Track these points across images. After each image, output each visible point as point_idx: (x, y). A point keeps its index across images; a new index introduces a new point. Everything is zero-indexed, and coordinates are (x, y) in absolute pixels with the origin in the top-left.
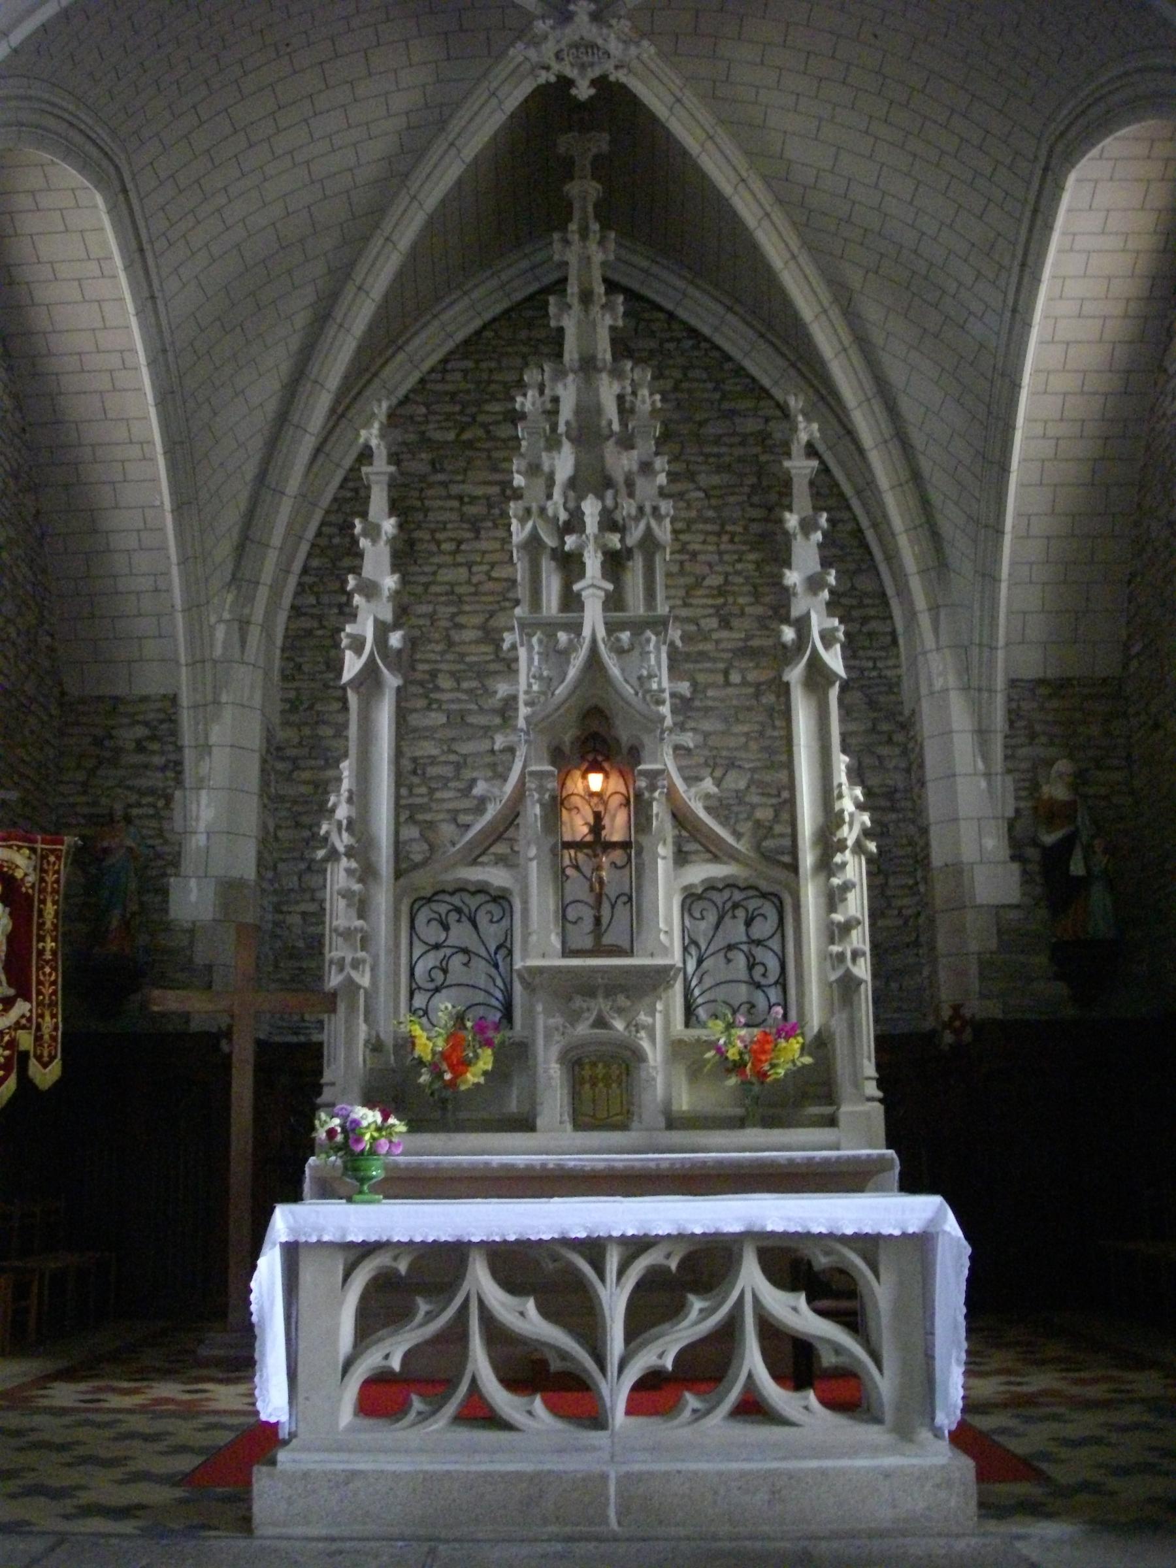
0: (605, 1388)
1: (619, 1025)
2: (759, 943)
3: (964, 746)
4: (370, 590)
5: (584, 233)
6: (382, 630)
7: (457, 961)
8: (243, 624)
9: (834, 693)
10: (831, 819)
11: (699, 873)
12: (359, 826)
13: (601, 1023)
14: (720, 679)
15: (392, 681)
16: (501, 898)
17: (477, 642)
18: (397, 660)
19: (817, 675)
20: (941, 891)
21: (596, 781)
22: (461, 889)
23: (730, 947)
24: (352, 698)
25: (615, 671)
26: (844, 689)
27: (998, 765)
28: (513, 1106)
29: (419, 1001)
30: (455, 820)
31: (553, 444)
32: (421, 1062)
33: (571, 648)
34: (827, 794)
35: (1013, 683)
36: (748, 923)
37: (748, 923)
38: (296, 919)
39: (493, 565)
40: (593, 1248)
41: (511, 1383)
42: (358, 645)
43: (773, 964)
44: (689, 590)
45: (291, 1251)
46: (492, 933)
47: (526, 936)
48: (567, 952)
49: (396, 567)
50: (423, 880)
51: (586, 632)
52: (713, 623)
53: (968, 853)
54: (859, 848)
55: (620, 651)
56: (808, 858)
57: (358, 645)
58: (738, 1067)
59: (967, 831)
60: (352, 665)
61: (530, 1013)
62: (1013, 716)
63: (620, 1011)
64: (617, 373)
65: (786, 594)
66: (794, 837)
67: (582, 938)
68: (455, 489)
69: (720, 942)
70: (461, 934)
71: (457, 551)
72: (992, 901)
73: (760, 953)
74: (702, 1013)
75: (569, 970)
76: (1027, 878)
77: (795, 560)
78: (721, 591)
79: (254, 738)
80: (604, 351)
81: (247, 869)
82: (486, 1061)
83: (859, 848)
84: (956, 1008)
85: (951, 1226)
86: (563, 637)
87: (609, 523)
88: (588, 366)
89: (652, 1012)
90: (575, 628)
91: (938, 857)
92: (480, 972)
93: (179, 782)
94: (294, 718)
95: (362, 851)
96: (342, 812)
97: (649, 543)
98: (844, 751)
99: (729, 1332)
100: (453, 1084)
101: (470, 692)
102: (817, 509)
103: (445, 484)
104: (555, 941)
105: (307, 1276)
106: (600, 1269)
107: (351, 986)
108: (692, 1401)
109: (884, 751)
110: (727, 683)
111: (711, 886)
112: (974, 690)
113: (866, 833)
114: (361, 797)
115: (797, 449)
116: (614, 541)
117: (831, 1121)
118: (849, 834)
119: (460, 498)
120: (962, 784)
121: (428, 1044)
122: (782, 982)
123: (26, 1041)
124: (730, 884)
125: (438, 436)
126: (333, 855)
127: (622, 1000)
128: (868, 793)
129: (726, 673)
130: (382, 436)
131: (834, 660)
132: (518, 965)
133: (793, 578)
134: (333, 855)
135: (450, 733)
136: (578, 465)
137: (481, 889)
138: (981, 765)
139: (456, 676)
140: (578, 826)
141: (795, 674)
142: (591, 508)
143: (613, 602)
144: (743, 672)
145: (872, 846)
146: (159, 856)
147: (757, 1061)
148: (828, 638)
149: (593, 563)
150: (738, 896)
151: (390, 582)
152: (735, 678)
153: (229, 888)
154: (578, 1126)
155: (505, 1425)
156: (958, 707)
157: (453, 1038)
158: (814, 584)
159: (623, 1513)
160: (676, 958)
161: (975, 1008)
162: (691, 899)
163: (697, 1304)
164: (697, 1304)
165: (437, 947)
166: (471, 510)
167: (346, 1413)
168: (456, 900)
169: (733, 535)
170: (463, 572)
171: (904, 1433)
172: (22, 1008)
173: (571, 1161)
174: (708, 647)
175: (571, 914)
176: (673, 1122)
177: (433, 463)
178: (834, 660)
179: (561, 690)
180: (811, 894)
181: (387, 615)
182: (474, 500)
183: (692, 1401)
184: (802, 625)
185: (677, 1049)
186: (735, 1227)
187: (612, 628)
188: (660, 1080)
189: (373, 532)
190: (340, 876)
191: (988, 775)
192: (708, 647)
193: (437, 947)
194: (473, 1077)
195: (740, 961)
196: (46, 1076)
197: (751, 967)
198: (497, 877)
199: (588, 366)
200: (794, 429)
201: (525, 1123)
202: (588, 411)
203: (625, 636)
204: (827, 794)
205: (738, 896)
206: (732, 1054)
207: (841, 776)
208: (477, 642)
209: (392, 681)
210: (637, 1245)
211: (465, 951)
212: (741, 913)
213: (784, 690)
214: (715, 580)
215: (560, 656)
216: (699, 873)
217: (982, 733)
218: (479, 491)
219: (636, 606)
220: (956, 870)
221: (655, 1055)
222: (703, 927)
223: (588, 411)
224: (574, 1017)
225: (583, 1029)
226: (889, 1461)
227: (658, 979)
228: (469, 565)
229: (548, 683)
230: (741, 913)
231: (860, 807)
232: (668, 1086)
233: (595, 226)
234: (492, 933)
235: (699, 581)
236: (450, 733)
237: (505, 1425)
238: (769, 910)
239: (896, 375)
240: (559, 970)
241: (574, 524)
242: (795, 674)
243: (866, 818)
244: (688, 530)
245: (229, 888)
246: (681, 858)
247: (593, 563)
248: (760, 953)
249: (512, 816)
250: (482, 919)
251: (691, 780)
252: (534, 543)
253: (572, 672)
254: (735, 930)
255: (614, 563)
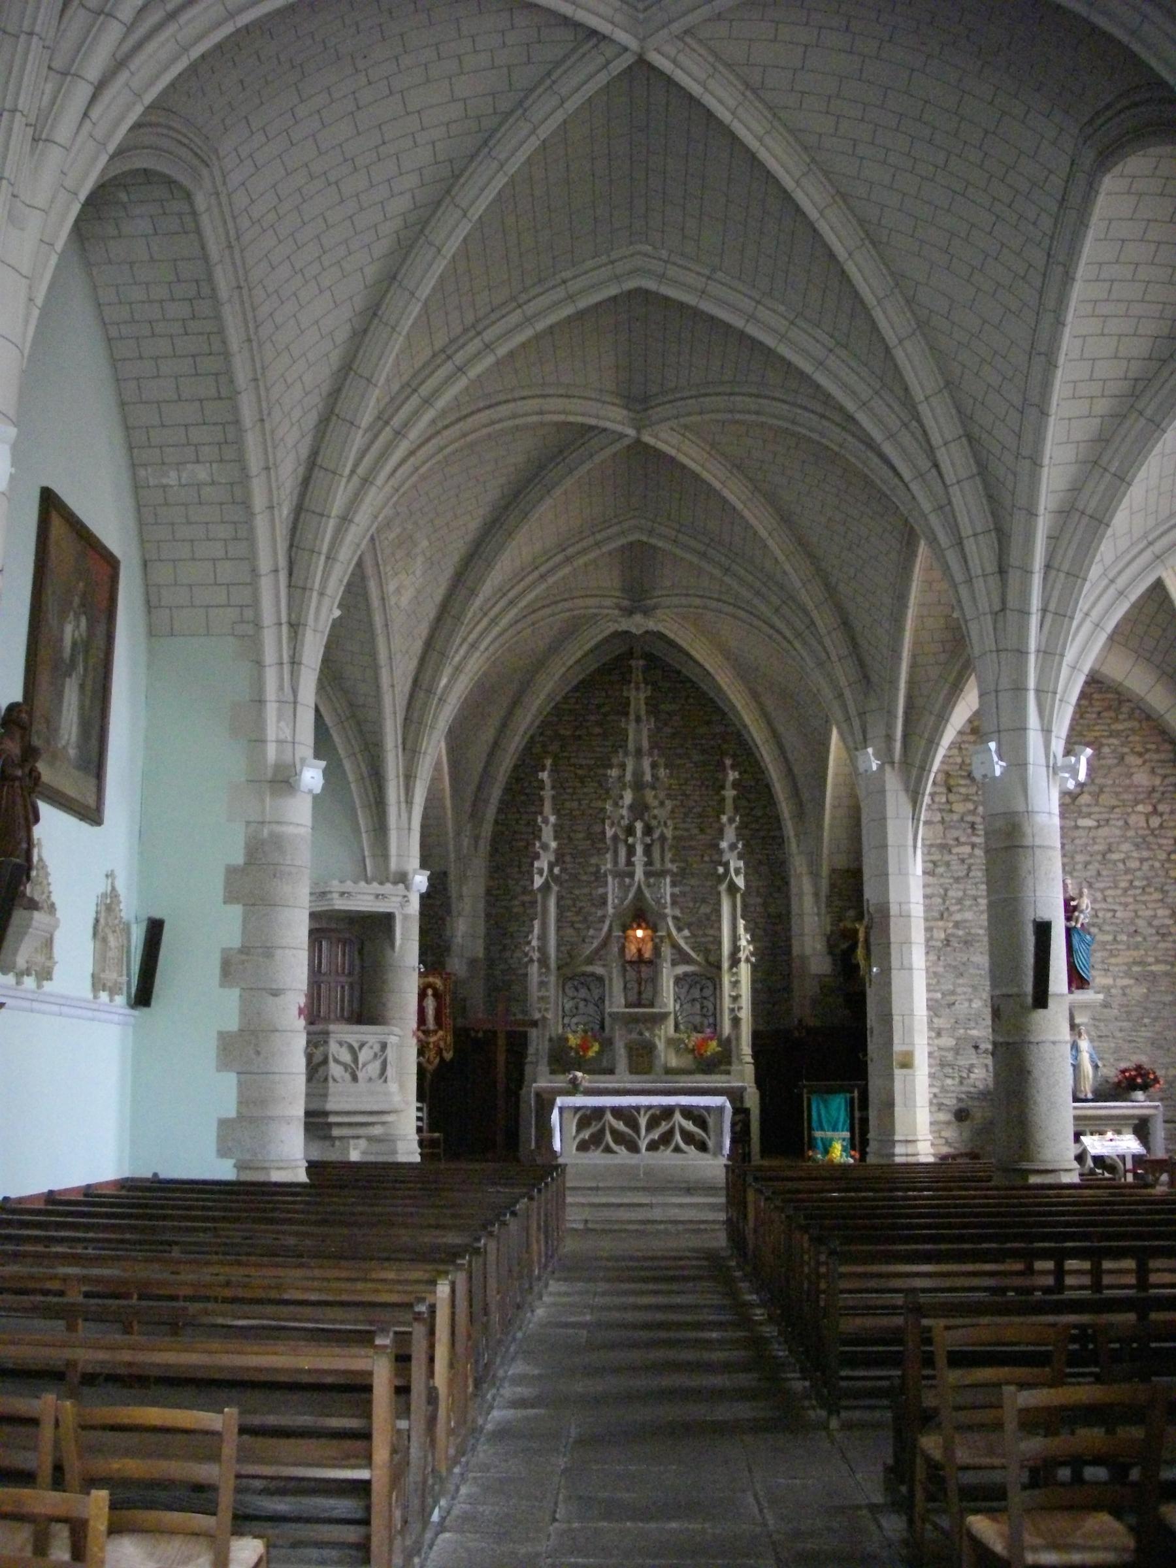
0: (640, 1143)
1: (647, 1034)
2: (705, 998)
3: (808, 903)
4: (545, 847)
5: (638, 689)
6: (551, 866)
7: (582, 1004)
8: (477, 838)
9: (739, 896)
10: (736, 949)
11: (681, 969)
12: (542, 949)
13: (641, 1034)
14: (698, 858)
15: (555, 888)
16: (600, 979)
17: (584, 839)
18: (556, 879)
19: (733, 889)
20: (796, 964)
21: (640, 933)
22: (584, 974)
23: (694, 1000)
24: (539, 897)
25: (648, 895)
26: (743, 896)
27: (823, 911)
28: (605, 1064)
29: (566, 1021)
30: (572, 926)
31: (623, 788)
32: (571, 1048)
33: (630, 886)
34: (735, 938)
35: (833, 871)
36: (701, 990)
37: (701, 990)
38: (498, 972)
39: (591, 801)
40: (637, 1109)
41: (616, 1142)
42: (541, 872)
43: (711, 1007)
44: (686, 815)
45: (561, 1109)
46: (596, 993)
47: (611, 996)
48: (626, 1006)
49: (556, 838)
50: (567, 971)
51: (636, 879)
52: (696, 831)
53: (808, 951)
54: (747, 960)
55: (649, 886)
56: (726, 965)
57: (541, 872)
58: (693, 1051)
59: (808, 941)
60: (538, 881)
61: (612, 1029)
62: (833, 886)
63: (648, 1029)
64: (651, 754)
65: (720, 852)
66: (720, 955)
67: (633, 997)
68: (572, 761)
69: (690, 997)
70: (583, 993)
71: (574, 793)
72: (819, 972)
73: (706, 1003)
74: (682, 1027)
75: (630, 1014)
76: (834, 963)
77: (725, 836)
78: (700, 816)
79: (481, 890)
80: (645, 745)
81: (481, 954)
82: (596, 1047)
83: (747, 960)
84: (800, 1021)
85: (728, 1104)
86: (627, 880)
87: (648, 831)
88: (639, 753)
89: (660, 1029)
90: (631, 875)
91: (796, 950)
92: (591, 1009)
93: (449, 912)
94: (496, 875)
95: (544, 962)
96: (535, 943)
97: (663, 838)
98: (743, 917)
99: (671, 1132)
100: (584, 1056)
101: (579, 863)
102: (735, 814)
103: (569, 758)
104: (623, 1001)
105: (565, 1115)
106: (639, 1113)
107: (544, 1018)
108: (662, 1148)
109: (776, 895)
110: (703, 862)
111: (686, 975)
112: (815, 875)
113: (752, 954)
114: (543, 937)
115: (728, 784)
116: (648, 840)
117: (728, 1073)
118: (742, 955)
119: (574, 765)
120: (807, 919)
121: (573, 1040)
122: (714, 1015)
123: (442, 1044)
124: (694, 974)
125: (562, 732)
126: (532, 960)
127: (649, 1025)
128: (752, 936)
129: (702, 856)
130: (549, 776)
131: (740, 882)
132: (608, 1010)
133: (724, 845)
134: (532, 960)
135: (571, 884)
136: (634, 799)
137: (593, 974)
138: (815, 910)
139: (574, 857)
140: (632, 949)
141: (723, 887)
142: (639, 826)
143: (649, 863)
144: (711, 856)
145: (753, 959)
146: (439, 946)
147: (699, 1049)
148: (737, 872)
149: (639, 849)
150: (697, 979)
151: (553, 845)
152: (706, 858)
153: (473, 962)
154: (631, 1072)
155: (615, 1152)
156: (807, 886)
157: (584, 1039)
158: (733, 847)
159: (645, 1174)
160: (671, 1009)
161: (812, 1022)
162: (678, 980)
163: (664, 1123)
164: (664, 1123)
165: (573, 998)
166: (580, 772)
167: (574, 1151)
168: (582, 979)
169: (707, 787)
170: (575, 804)
171: (715, 1155)
172: (441, 1033)
173: (628, 1086)
174: (693, 843)
175: (629, 986)
176: (669, 1071)
177: (562, 746)
178: (740, 882)
179: (626, 902)
180: (726, 979)
181: (552, 859)
182: (581, 766)
183: (662, 1148)
184: (726, 865)
185: (670, 1042)
186: (673, 1103)
187: (648, 874)
188: (663, 1055)
189: (546, 821)
190: (534, 969)
191: (818, 914)
192: (693, 843)
193: (573, 998)
194: (591, 1054)
195: (698, 1006)
196: (448, 1056)
197: (702, 1008)
198: (599, 970)
199: (639, 753)
200: (726, 775)
201: (611, 1072)
202: (638, 774)
203: (652, 880)
204: (735, 938)
205: (697, 979)
206: (690, 1046)
207: (741, 930)
208: (584, 839)
209: (555, 888)
210: (649, 1108)
211: (585, 1000)
212: (698, 986)
213: (719, 893)
214: (698, 810)
215: (626, 889)
216: (681, 969)
217: (816, 895)
218: (584, 762)
219: (658, 866)
220: (803, 958)
221: (661, 1045)
222: (684, 991)
223: (638, 774)
224: (630, 1032)
225: (634, 1036)
226: (711, 1162)
227: (664, 1016)
228: (579, 800)
229: (622, 900)
230: (698, 986)
231: (749, 942)
232: (666, 1056)
233: (642, 685)
234: (596, 993)
235: (691, 809)
236: (571, 884)
237: (615, 1152)
238: (709, 984)
239: (781, 729)
240: (623, 1013)
241: (630, 831)
242: (723, 887)
243: (751, 948)
244: (686, 784)
245: (473, 962)
246: (674, 963)
247: (639, 849)
248: (706, 1003)
249: (605, 944)
250: (592, 987)
251: (679, 930)
252: (615, 837)
253: (631, 896)
254: (696, 993)
255: (648, 850)
